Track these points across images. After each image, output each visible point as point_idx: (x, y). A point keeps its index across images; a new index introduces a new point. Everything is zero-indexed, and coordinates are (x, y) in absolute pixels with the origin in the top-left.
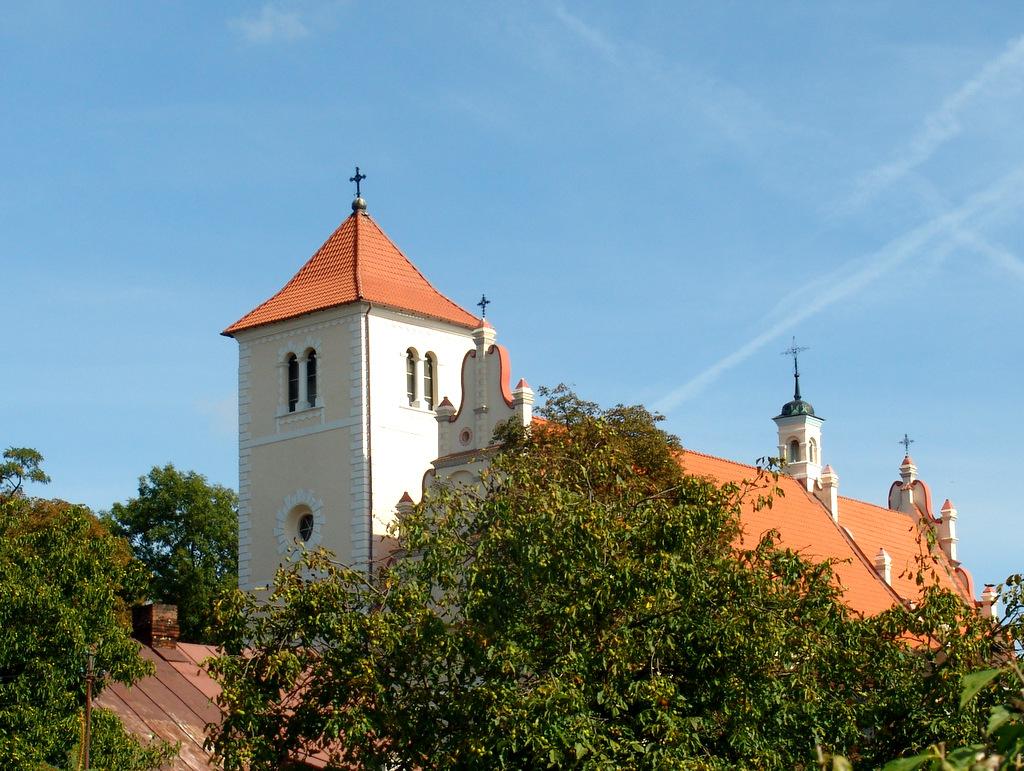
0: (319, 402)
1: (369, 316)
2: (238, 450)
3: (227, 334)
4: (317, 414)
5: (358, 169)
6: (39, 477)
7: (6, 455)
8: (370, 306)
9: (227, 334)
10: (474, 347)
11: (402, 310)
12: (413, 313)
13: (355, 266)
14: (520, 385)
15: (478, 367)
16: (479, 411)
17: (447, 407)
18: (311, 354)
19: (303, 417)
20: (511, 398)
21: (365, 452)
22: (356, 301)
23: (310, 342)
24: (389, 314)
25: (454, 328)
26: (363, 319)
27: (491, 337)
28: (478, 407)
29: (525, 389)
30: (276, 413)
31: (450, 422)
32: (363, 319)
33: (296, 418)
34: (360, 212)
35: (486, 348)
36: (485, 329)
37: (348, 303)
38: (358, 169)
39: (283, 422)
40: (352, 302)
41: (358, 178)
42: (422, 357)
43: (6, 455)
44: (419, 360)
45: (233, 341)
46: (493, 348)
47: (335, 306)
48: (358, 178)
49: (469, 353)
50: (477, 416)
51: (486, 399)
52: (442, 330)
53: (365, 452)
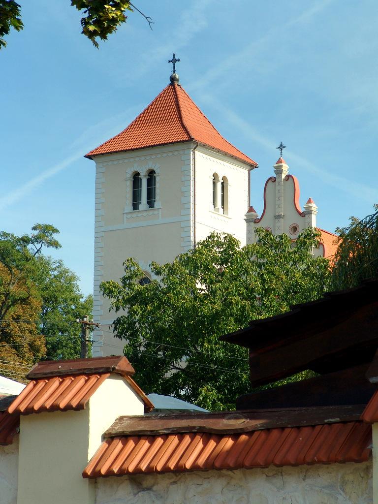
0: (157, 205)
1: (196, 151)
2: (94, 233)
3: (89, 157)
4: (156, 212)
5: (174, 55)
6: (55, 245)
7: (34, 228)
8: (197, 145)
9: (89, 157)
10: (275, 175)
11: (213, 149)
12: (219, 151)
13: (180, 118)
14: (309, 201)
15: (277, 188)
16: (278, 217)
17: (253, 213)
18: (151, 174)
19: (145, 214)
20: (302, 210)
21: (192, 239)
22: (188, 141)
23: (151, 166)
24: (206, 150)
25: (238, 163)
26: (192, 153)
27: (286, 169)
28: (277, 214)
29: (313, 205)
30: (124, 211)
31: (255, 222)
32: (192, 153)
33: (140, 215)
34: (176, 83)
35: (283, 176)
36: (283, 164)
37: (183, 141)
38: (174, 55)
39: (129, 216)
40: (186, 141)
41: (174, 61)
42: (220, 179)
43: (34, 228)
44: (219, 181)
45: (92, 163)
46: (289, 177)
47: (111, 153)
48: (174, 61)
49: (270, 179)
50: (277, 220)
51: (283, 209)
52: (235, 164)
53: (192, 239)
